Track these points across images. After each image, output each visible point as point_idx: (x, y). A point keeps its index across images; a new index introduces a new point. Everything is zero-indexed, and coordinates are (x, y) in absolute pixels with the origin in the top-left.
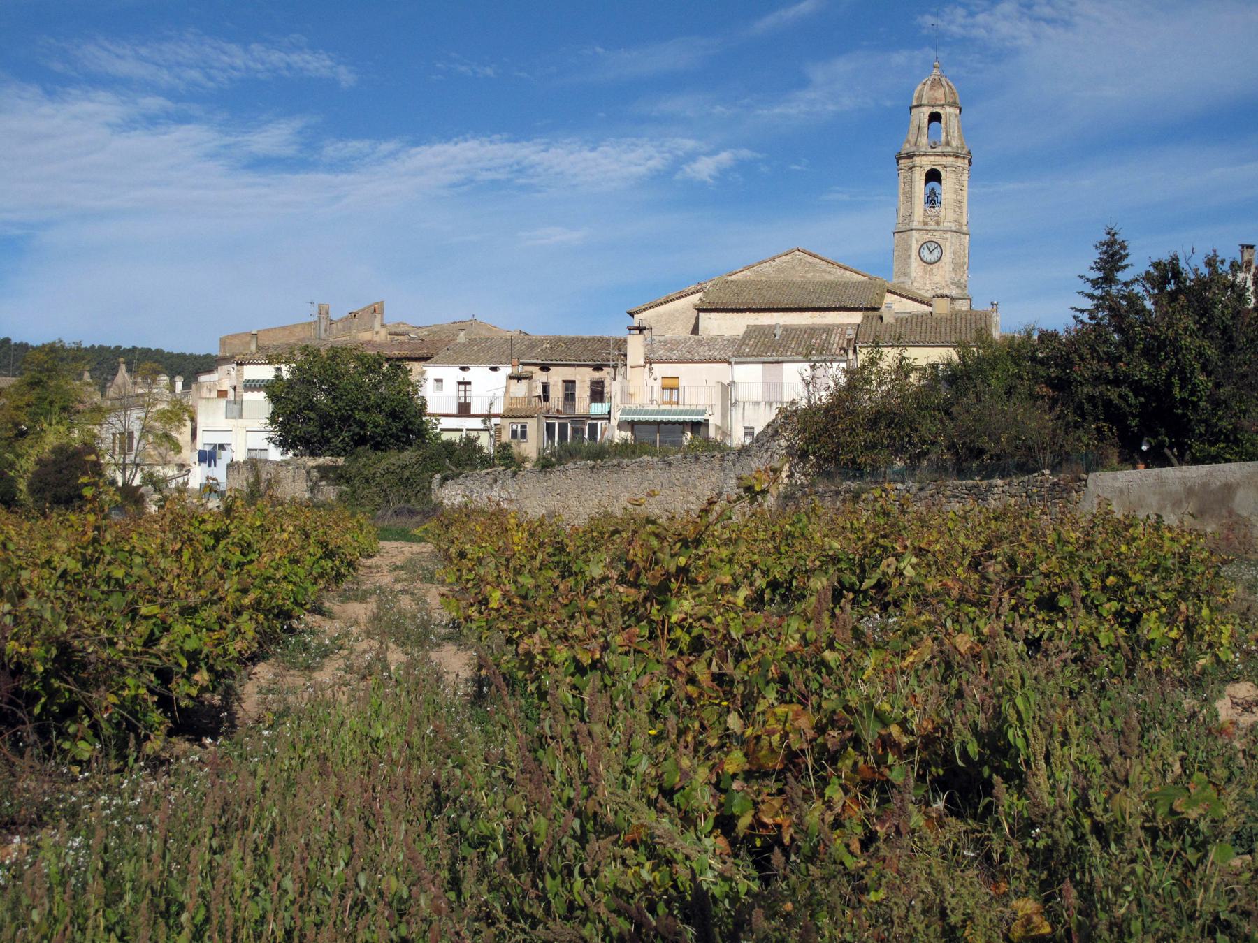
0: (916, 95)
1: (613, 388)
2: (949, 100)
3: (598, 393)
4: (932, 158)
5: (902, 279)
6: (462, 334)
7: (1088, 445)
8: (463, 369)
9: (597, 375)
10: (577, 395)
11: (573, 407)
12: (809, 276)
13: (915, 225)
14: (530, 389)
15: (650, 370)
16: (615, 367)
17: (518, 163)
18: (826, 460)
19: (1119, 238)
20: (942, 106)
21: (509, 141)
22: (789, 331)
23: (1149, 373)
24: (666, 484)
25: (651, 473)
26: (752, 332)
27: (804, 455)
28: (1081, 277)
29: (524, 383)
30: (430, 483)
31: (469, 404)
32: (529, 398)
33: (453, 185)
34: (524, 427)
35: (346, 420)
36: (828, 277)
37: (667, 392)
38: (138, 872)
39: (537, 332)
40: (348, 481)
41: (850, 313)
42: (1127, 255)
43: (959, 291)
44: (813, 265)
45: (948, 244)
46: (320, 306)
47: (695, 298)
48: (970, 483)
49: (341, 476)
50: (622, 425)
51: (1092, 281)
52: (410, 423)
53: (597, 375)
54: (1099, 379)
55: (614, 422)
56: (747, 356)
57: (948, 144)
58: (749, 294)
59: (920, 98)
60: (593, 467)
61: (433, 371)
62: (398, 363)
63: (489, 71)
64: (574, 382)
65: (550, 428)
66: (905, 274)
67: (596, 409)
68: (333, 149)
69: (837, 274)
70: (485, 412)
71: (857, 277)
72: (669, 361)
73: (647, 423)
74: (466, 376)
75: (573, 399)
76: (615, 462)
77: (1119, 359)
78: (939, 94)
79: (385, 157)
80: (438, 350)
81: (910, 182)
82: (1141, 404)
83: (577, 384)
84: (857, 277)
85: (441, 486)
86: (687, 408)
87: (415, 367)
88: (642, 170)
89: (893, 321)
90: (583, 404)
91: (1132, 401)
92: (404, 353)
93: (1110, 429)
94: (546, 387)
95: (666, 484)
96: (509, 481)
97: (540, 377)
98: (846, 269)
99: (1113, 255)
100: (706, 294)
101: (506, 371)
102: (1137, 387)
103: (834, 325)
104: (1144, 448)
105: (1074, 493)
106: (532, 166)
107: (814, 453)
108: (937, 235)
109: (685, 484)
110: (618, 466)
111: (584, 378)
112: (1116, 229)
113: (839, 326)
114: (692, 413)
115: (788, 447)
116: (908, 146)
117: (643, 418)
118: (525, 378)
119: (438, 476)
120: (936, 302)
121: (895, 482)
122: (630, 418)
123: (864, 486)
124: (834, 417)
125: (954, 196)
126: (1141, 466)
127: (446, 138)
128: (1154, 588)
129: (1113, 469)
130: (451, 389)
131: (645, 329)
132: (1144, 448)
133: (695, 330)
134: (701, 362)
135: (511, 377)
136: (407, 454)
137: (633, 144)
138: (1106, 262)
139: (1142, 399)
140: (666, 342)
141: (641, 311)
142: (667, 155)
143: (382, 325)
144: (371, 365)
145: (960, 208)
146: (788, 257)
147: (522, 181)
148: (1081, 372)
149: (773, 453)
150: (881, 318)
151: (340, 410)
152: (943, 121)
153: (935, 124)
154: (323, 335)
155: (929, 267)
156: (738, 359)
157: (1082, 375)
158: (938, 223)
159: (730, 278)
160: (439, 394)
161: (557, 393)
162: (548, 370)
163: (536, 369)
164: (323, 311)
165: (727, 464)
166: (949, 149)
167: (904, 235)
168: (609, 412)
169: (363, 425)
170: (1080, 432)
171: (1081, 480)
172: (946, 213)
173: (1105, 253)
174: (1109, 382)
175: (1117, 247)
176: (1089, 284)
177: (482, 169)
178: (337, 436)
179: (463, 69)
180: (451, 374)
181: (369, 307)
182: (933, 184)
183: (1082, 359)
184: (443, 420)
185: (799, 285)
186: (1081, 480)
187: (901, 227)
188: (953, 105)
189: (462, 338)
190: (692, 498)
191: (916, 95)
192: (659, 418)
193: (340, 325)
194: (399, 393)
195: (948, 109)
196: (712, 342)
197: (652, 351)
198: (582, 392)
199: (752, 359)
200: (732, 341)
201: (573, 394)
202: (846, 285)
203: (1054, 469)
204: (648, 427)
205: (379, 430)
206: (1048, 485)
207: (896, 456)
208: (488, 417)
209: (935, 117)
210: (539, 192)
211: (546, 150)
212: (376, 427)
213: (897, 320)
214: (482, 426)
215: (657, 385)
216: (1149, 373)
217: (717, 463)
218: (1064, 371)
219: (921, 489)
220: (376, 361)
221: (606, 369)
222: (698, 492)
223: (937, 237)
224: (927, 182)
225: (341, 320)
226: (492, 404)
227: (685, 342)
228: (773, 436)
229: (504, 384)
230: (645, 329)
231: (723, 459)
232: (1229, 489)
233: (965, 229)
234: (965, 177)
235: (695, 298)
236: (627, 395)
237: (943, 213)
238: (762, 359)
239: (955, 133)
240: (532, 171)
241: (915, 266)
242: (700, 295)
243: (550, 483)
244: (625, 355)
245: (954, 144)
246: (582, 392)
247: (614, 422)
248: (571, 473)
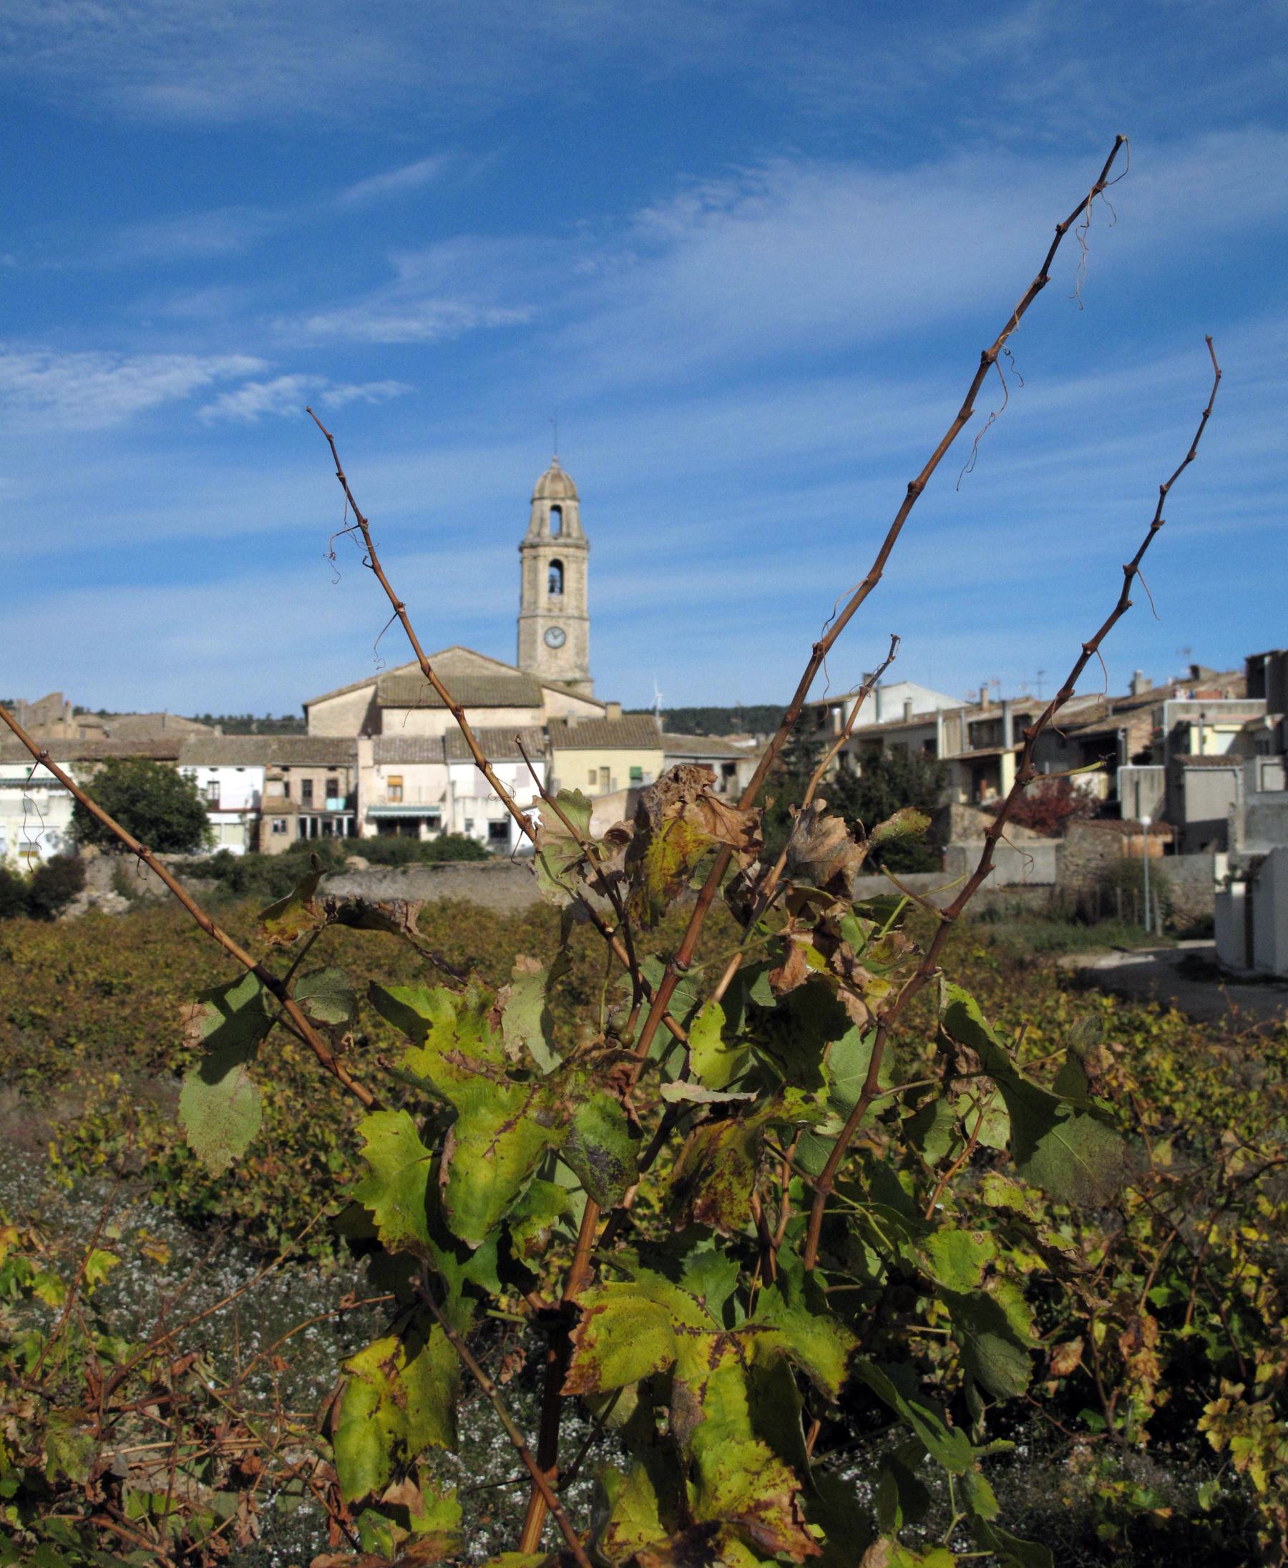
4: (555, 549)
8: (212, 770)
9: (332, 775)
34: (284, 822)
36: (486, 673)
38: (1199, 1070)
44: (471, 661)
53: (332, 775)
57: (569, 535)
59: (542, 489)
72: (392, 762)
78: (560, 487)
81: (535, 571)
98: (502, 665)
111: (320, 777)
122: (377, 814)
134: (421, 762)
145: (581, 595)
146: (449, 654)
155: (554, 652)
158: (561, 610)
161: (297, 793)
166: (569, 541)
167: (530, 621)
172: (569, 600)
188: (574, 498)
215: (384, 783)
221: (340, 770)
223: (561, 623)
232: (924, 887)
233: (585, 615)
234: (585, 567)
239: (574, 525)
241: (541, 651)
245: (575, 534)
246: (319, 791)
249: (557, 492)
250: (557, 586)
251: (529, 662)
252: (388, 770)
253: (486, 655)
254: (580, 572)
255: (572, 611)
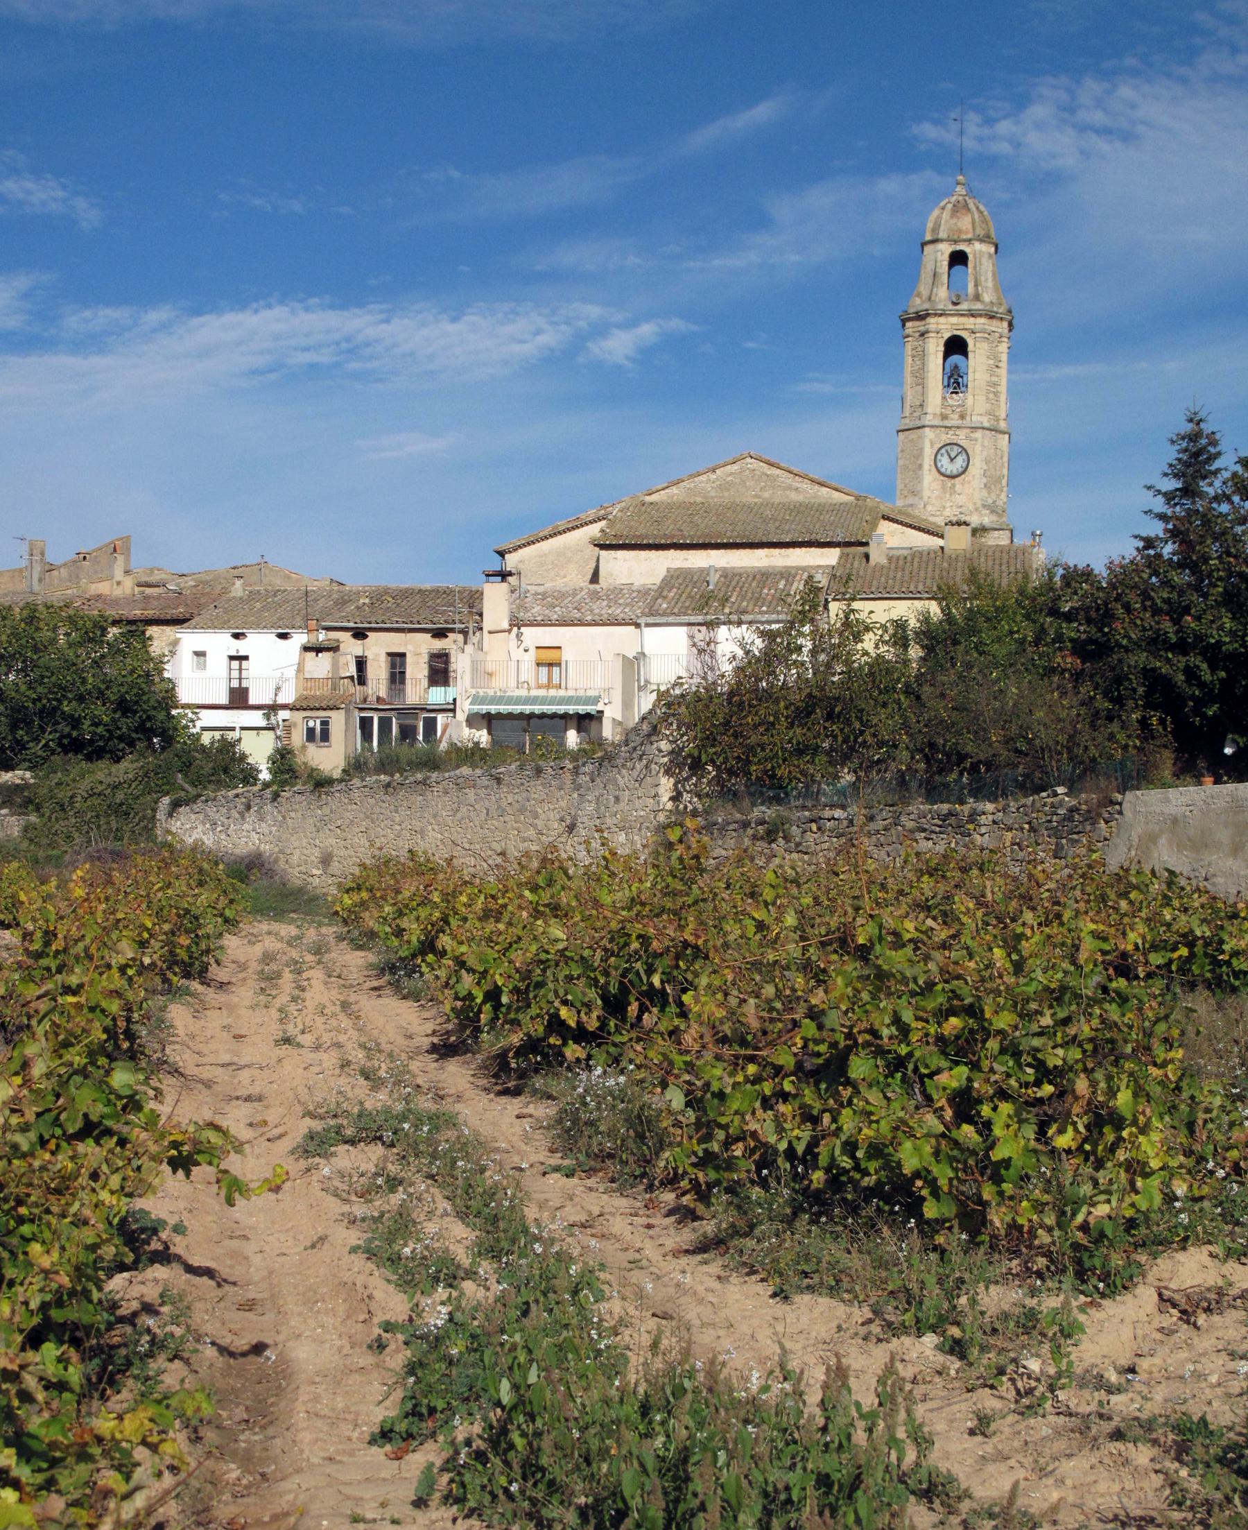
0: (930, 225)
1: (461, 663)
2: (980, 232)
3: (440, 672)
4: (954, 320)
5: (910, 500)
6: (238, 583)
7: (1125, 747)
8: (237, 636)
9: (438, 645)
10: (408, 675)
11: (402, 691)
12: (766, 495)
13: (928, 420)
14: (335, 665)
15: (519, 636)
16: (464, 632)
17: (348, 340)
18: (731, 772)
19: (1207, 428)
20: (969, 241)
21: (332, 307)
22: (728, 575)
23: (1232, 633)
24: (494, 813)
25: (471, 794)
26: (674, 578)
27: (696, 766)
28: (1149, 488)
29: (325, 657)
30: (154, 810)
31: (247, 689)
32: (335, 680)
33: (255, 372)
35: (49, 714)
36: (794, 497)
37: (544, 670)
39: (354, 583)
40: (38, 808)
41: (826, 550)
42: (1219, 454)
43: (994, 518)
45: (978, 448)
46: (31, 543)
47: (594, 530)
48: (945, 807)
49: (29, 801)
50: (472, 720)
51: (1165, 494)
52: (149, 718)
53: (438, 645)
54: (1156, 643)
55: (461, 716)
56: (664, 614)
57: (977, 297)
58: (675, 523)
59: (936, 229)
60: (388, 785)
61: (190, 640)
62: (136, 628)
63: (297, 206)
64: (403, 655)
65: (365, 724)
66: (914, 493)
67: (437, 695)
68: (76, 320)
69: (808, 492)
70: (268, 701)
71: (838, 497)
73: (510, 716)
74: (241, 647)
75: (403, 681)
76: (419, 776)
77: (1187, 610)
78: (965, 223)
79: (154, 331)
80: (200, 607)
81: (922, 355)
82: (1221, 680)
83: (409, 659)
84: (838, 497)
85: (170, 815)
86: (571, 693)
87: (159, 637)
88: (528, 349)
89: (884, 561)
90: (418, 690)
91: (1207, 676)
92: (150, 613)
93: (1162, 722)
94: (361, 663)
95: (494, 813)
96: (268, 808)
97: (351, 647)
98: (822, 484)
99: (1196, 455)
100: (612, 524)
101: (300, 639)
102: (1213, 654)
103: (798, 568)
104: (1228, 751)
105: (1102, 824)
106: (368, 345)
107: (713, 762)
108: (962, 434)
109: (522, 811)
110: (424, 782)
111: (418, 648)
112: (1202, 414)
113: (804, 569)
114: (578, 701)
115: (672, 752)
116: (918, 301)
117: (504, 709)
118: (328, 649)
119: (166, 800)
120: (951, 532)
121: (832, 806)
122: (484, 708)
123: (785, 814)
124: (741, 704)
125: (986, 377)
126: (1208, 780)
127: (241, 303)
128: (1036, 1042)
129: (1164, 786)
130: (218, 666)
131: (510, 574)
132: (1228, 751)
133: (595, 578)
134: (594, 623)
135: (306, 649)
136: (124, 765)
137: (513, 312)
138: (1187, 465)
139: (1223, 674)
140: (544, 595)
141: (516, 549)
142: (563, 327)
143: (127, 572)
144: (92, 631)
145: (996, 394)
146: (735, 467)
147: (354, 365)
148: (1123, 630)
149: (650, 762)
150: (867, 557)
151: (39, 699)
152: (970, 264)
153: (958, 268)
154: (36, 587)
155: (949, 483)
156: (650, 620)
157: (1126, 636)
158: (962, 417)
159: (648, 499)
160: (200, 674)
161: (378, 672)
162: (365, 637)
163: (345, 637)
164: (36, 551)
165: (583, 779)
166: (978, 306)
167: (912, 435)
168: (455, 700)
169: (75, 722)
170: (1115, 727)
171: (1112, 803)
172: (976, 401)
173: (1186, 450)
174: (1171, 647)
175: (1204, 441)
176: (1160, 500)
177: (296, 349)
178: (36, 740)
179: (257, 202)
180: (219, 644)
181: (107, 545)
182: (956, 359)
183: (1128, 608)
184: (204, 714)
185: (749, 508)
186: (1112, 803)
187: (908, 423)
188: (985, 239)
189: (238, 589)
190: (531, 833)
191: (930, 225)
192: (527, 709)
193: (64, 572)
194: (133, 671)
195: (978, 246)
196: (615, 594)
197: (522, 607)
198: (417, 671)
199: (671, 619)
200: (644, 593)
201: (403, 673)
202: (821, 508)
203: (1073, 786)
204: (508, 723)
205: (100, 730)
206: (1062, 811)
207: (843, 765)
208: (273, 708)
209: (959, 259)
210: (380, 380)
211: (387, 321)
212: (96, 725)
213: (890, 559)
214: (263, 723)
215: (529, 659)
216: (1232, 633)
217: (567, 777)
218: (1100, 630)
219: (871, 818)
220: (96, 625)
222: (540, 823)
223: (961, 437)
224: (947, 355)
225: (65, 564)
226: (278, 689)
227: (574, 594)
228: (649, 735)
229: (296, 659)
230: (510, 574)
231: (576, 771)
233: (1003, 425)
234: (1004, 347)
235: (594, 530)
236: (482, 674)
237: (970, 401)
238: (686, 619)
239: (988, 282)
240: (369, 351)
242: (603, 523)
243: (326, 810)
244: (481, 615)
245: (987, 297)
246: (417, 671)
247: (461, 716)
248: (356, 795)
249: (960, 231)
250: (955, 381)
251: (910, 500)
252: (534, 636)
253: (796, 470)
254: (995, 357)
255: (976, 420)
